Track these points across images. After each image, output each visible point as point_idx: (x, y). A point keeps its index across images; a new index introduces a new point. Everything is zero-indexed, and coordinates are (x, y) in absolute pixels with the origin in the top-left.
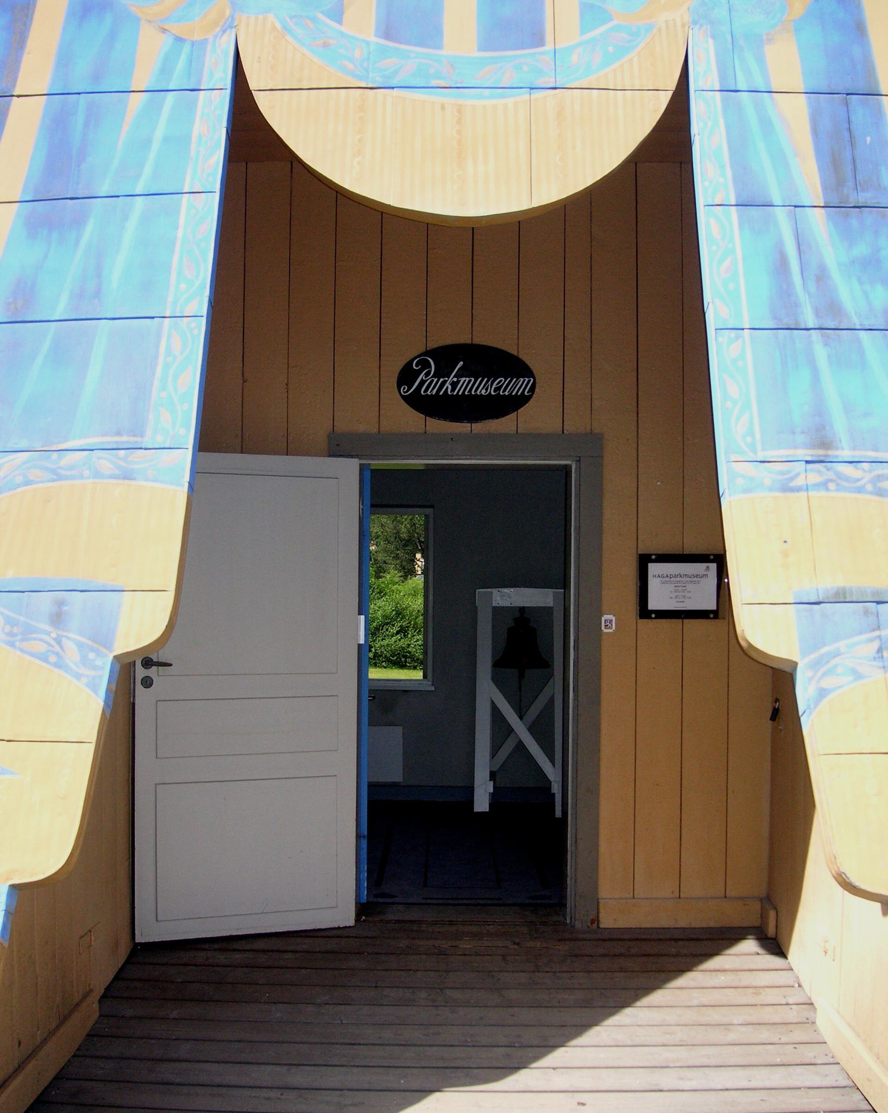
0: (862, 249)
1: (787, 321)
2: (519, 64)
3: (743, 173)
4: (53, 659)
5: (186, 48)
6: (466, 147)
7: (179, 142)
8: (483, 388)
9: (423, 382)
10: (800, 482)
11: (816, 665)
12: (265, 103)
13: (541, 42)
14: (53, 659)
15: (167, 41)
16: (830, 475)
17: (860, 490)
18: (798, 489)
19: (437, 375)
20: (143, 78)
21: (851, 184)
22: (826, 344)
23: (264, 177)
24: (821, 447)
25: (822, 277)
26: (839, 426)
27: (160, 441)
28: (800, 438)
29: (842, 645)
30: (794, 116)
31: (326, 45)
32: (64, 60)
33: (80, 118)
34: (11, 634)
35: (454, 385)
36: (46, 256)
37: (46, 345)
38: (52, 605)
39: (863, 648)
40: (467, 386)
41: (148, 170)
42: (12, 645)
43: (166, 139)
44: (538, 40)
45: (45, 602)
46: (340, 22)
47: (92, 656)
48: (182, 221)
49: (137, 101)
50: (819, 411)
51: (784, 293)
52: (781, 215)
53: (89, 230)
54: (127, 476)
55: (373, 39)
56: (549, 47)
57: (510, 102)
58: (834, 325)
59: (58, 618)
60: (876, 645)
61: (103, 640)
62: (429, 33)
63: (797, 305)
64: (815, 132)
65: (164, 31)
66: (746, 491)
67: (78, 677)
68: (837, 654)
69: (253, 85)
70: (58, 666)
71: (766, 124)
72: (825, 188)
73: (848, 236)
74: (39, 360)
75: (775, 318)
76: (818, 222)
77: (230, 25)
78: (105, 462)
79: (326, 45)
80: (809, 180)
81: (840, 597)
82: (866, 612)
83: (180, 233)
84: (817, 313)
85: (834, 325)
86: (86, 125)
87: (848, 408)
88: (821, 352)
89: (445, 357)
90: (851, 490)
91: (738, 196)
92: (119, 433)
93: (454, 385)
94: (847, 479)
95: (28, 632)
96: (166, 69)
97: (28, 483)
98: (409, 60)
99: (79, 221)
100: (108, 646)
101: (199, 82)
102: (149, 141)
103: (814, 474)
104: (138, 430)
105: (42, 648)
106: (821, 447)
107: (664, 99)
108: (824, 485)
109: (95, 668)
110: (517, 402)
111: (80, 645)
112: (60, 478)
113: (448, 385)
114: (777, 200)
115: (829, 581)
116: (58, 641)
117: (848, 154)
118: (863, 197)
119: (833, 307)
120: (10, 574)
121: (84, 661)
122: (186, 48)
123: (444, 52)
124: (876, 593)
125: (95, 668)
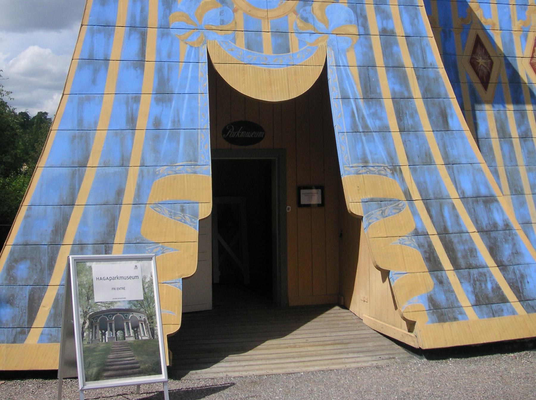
0: (372, 110)
1: (355, 130)
2: (284, 57)
3: (343, 90)
4: (183, 221)
5: (194, 49)
6: (272, 83)
7: (195, 78)
8: (249, 135)
9: (230, 133)
10: (361, 172)
11: (367, 217)
12: (217, 67)
13: (289, 52)
14: (183, 221)
15: (188, 46)
16: (368, 170)
17: (375, 174)
18: (360, 174)
19: (235, 131)
20: (183, 58)
21: (369, 92)
22: (365, 136)
23: (219, 90)
24: (365, 162)
25: (363, 118)
26: (369, 157)
27: (202, 163)
28: (360, 161)
29: (373, 212)
30: (354, 72)
31: (232, 50)
32: (159, 51)
33: (166, 69)
34: (170, 215)
35: (240, 134)
36: (162, 110)
37: (167, 136)
38: (181, 208)
39: (378, 212)
40: (243, 134)
41: (188, 86)
42: (171, 218)
43: (192, 77)
44: (288, 51)
45: (178, 206)
46: (235, 43)
47: (193, 220)
48: (199, 101)
49: (182, 65)
50: (364, 154)
51: (354, 123)
52: (352, 100)
53: (174, 103)
54: (195, 173)
55: (244, 49)
56: (291, 53)
57: (282, 69)
58: (367, 131)
59: (183, 210)
60: (381, 211)
61: (195, 215)
62: (260, 49)
63: (357, 126)
64: (360, 78)
65: (187, 44)
66: (348, 174)
67: (191, 225)
68: (372, 214)
69: (213, 61)
70: (184, 223)
71: (347, 75)
72: (363, 94)
73: (369, 107)
74: (165, 141)
75: (352, 129)
76: (361, 102)
77: (205, 43)
78: (188, 169)
79: (232, 50)
80: (358, 91)
81: (372, 200)
82: (378, 204)
83: (199, 105)
84: (362, 127)
85: (367, 131)
86: (168, 72)
87: (371, 152)
88: (364, 138)
89: (237, 125)
90: (373, 174)
91: (341, 96)
92: (191, 161)
93: (240, 134)
94: (372, 171)
95: (175, 214)
96: (189, 55)
97: (168, 175)
98: (254, 55)
99: (170, 100)
100: (197, 217)
101: (199, 60)
102: (187, 78)
103: (363, 170)
104: (196, 160)
105: (180, 218)
106: (365, 162)
107: (322, 68)
108: (366, 173)
109: (195, 223)
110: (261, 139)
111: (190, 217)
112: (176, 173)
113: (238, 134)
114: (351, 97)
115: (370, 196)
116: (184, 216)
117: (368, 84)
118: (373, 96)
119: (365, 126)
120: (168, 199)
121: (192, 222)
122: (194, 49)
123: (264, 54)
124: (380, 199)
125: (195, 223)
